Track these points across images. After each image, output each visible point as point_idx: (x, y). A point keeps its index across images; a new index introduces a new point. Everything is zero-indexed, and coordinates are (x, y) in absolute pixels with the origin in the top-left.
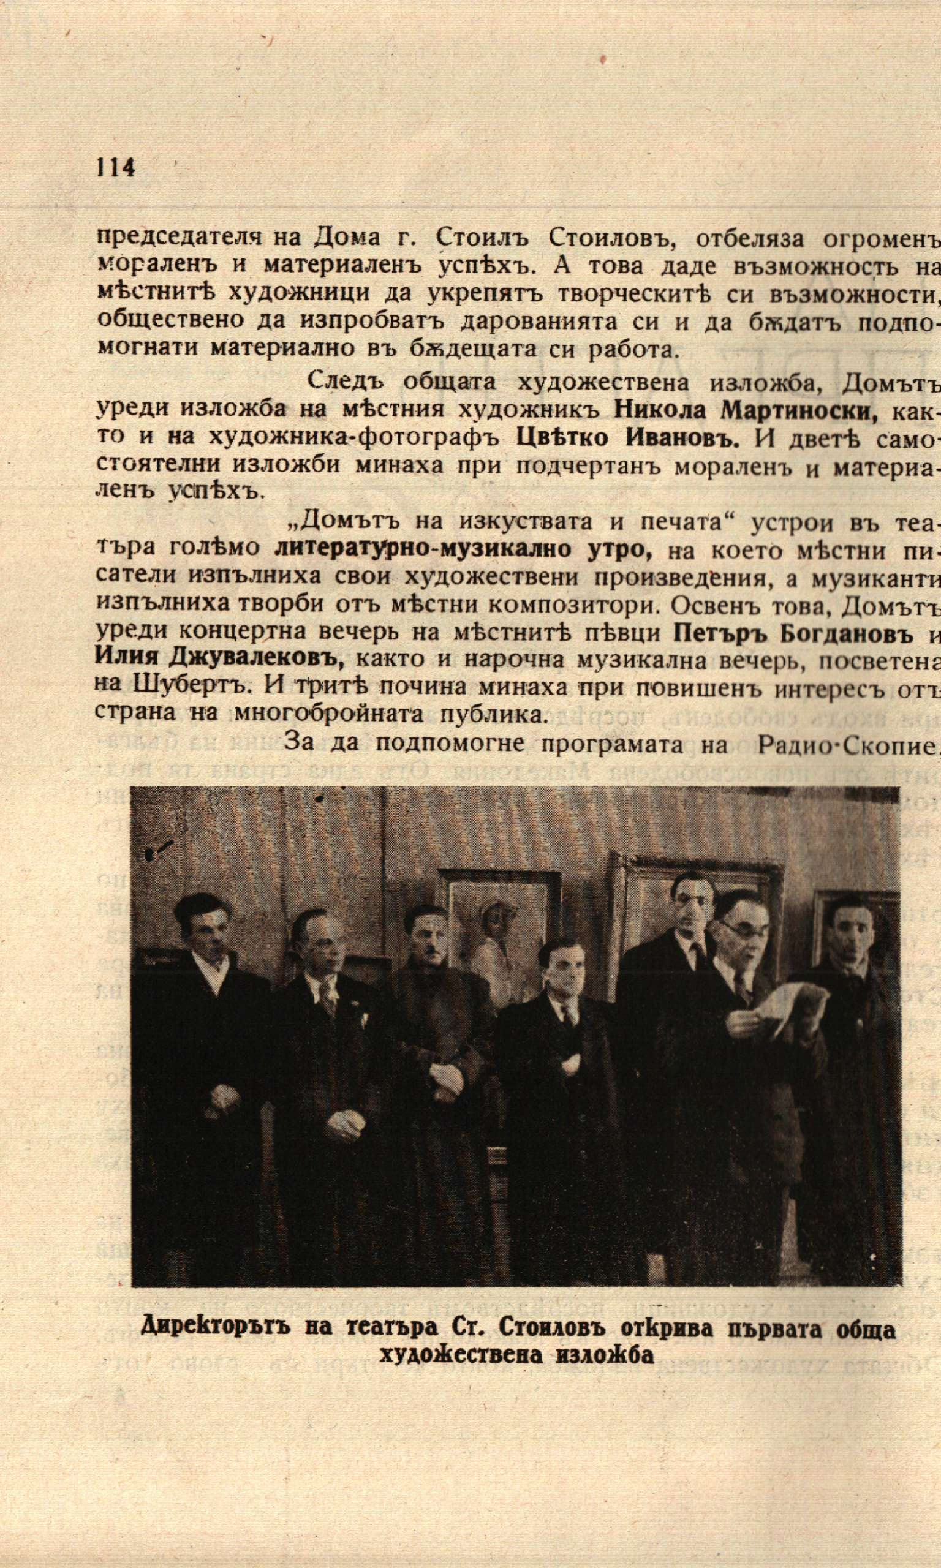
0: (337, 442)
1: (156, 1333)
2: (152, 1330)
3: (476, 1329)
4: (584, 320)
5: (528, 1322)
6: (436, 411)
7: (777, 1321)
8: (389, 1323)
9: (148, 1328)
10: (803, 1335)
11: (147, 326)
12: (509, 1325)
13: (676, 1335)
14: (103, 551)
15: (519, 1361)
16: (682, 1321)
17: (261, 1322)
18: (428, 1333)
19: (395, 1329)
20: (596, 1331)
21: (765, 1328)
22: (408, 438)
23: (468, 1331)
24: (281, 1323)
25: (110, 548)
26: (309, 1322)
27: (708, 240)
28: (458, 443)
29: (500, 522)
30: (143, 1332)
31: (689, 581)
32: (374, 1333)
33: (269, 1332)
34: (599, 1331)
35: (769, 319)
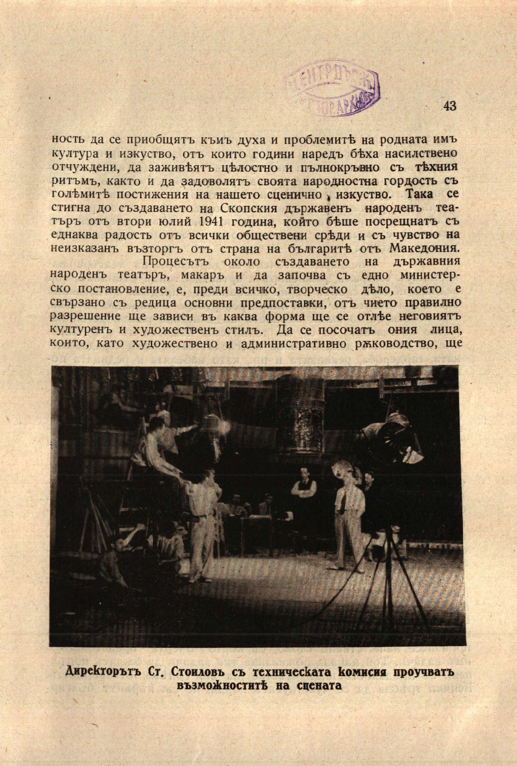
0: (428, 264)
1: (73, 675)
2: (71, 673)
3: (160, 673)
4: (177, 139)
6: (273, 209)
7: (213, 669)
8: (444, 670)
9: (69, 672)
10: (321, 675)
12: (176, 671)
15: (317, 689)
16: (78, 667)
17: (126, 670)
20: (122, 673)
21: (84, 670)
23: (179, 674)
24: (450, 670)
27: (366, 249)
28: (397, 157)
30: (67, 674)
33: (130, 674)
34: (242, 674)
35: (365, 342)
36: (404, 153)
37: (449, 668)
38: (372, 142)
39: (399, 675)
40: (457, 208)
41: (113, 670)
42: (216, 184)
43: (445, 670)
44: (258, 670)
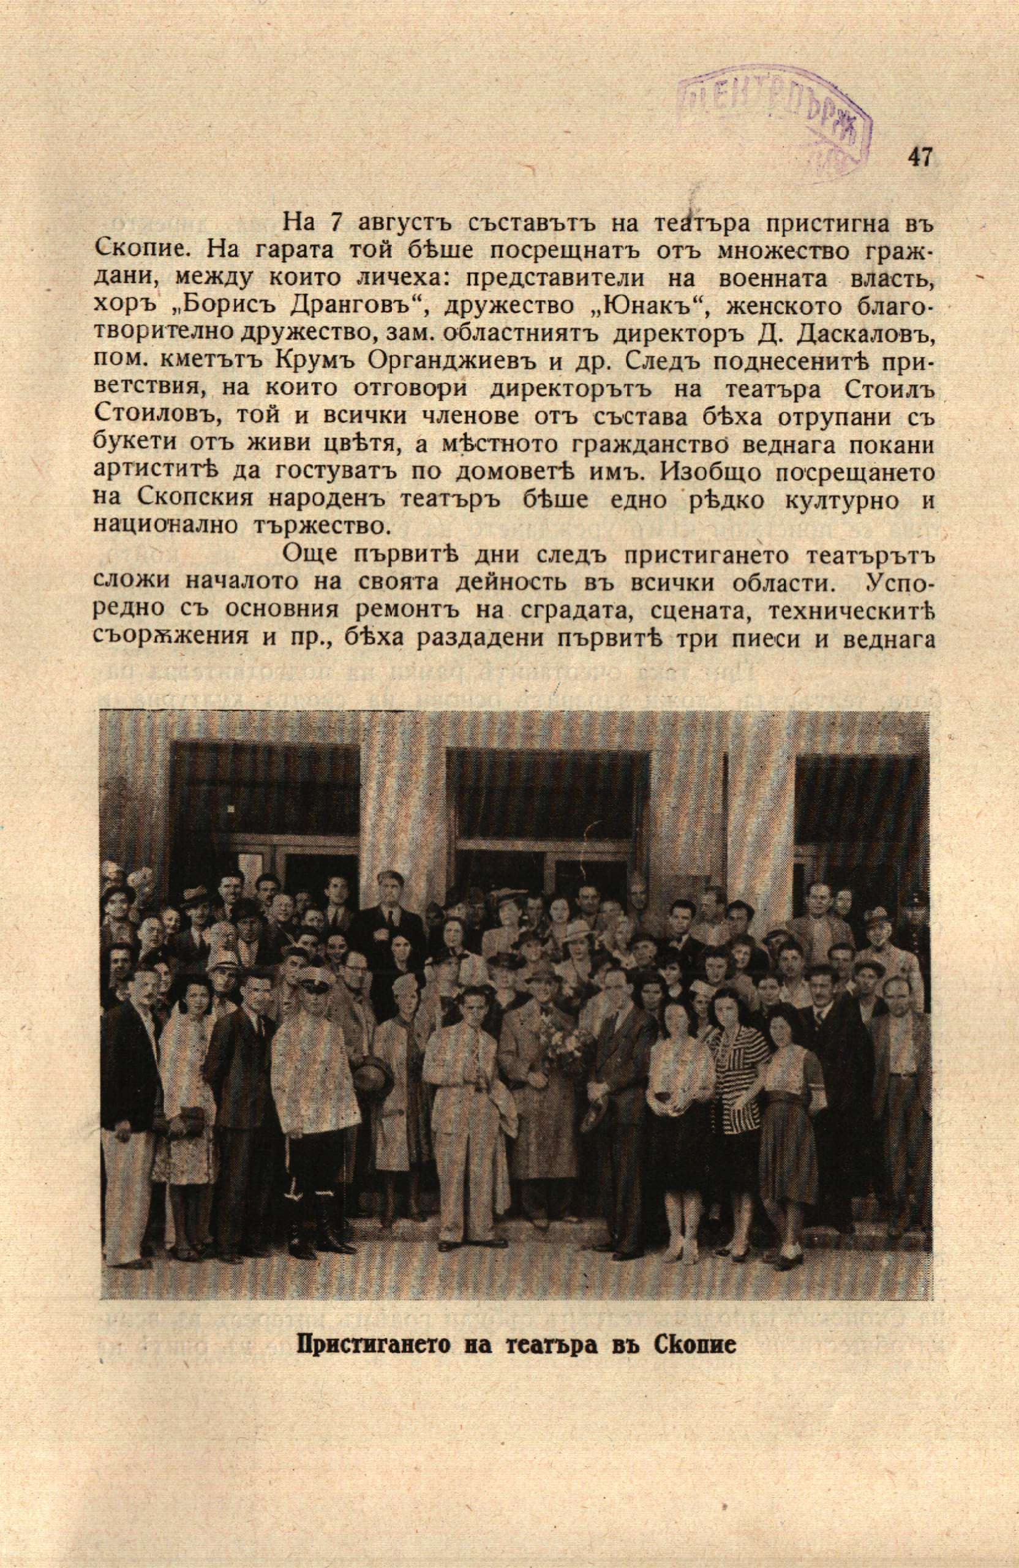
5: (440, 1339)
6: (191, 388)
8: (549, 1342)
11: (742, 479)
13: (329, 1351)
14: (260, 531)
18: (588, 1351)
19: (555, 1347)
20: (631, 1348)
22: (877, 391)
25: (266, 528)
26: (615, 1341)
29: (799, 502)
31: (763, 448)
32: (534, 1351)
34: (634, 1348)
36: (349, 414)
37: (559, 1337)
38: (634, 226)
39: (309, 1350)
40: (931, 364)
41: (697, 1344)
42: (120, 335)
43: (552, 1341)
44: (515, 1341)
